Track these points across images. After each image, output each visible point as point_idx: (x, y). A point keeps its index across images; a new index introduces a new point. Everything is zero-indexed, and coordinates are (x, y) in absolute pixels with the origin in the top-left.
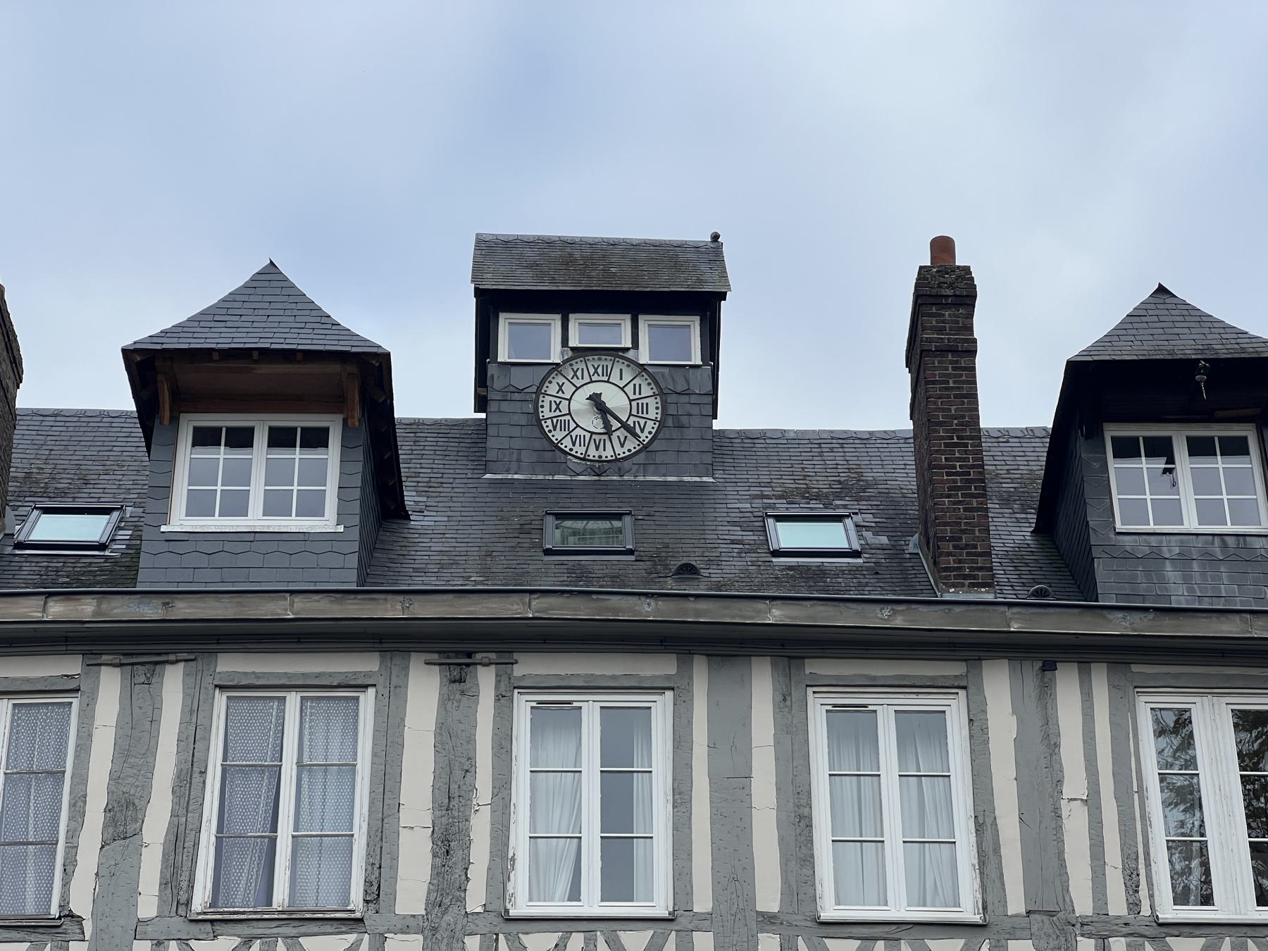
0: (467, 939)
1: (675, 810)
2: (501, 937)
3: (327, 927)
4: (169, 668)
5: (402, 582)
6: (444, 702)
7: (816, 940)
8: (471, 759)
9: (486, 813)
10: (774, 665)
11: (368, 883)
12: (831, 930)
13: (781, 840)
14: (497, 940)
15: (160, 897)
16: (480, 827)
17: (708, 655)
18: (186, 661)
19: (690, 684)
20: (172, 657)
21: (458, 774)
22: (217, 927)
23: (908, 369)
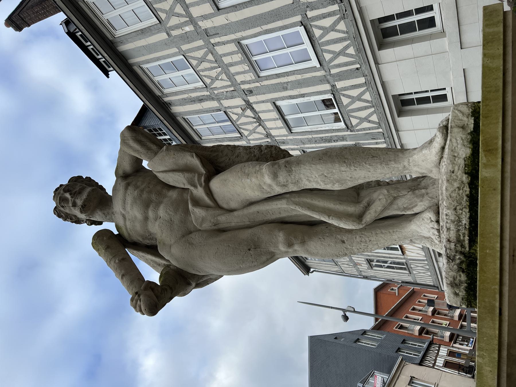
0: (216, 93)
1: (140, 32)
2: (211, 87)
3: (229, 117)
4: (165, 101)
5: (429, 356)
6: (176, 106)
7: (165, 23)
8: (182, 99)
9: (190, 95)
10: (118, 47)
11: (217, 111)
12: (160, 19)
13: (150, 36)
14: (212, 88)
15: (241, 141)
16: (194, 95)
17: (127, 60)
18: (161, 98)
19: (137, 63)
20: (162, 101)
21: (187, 101)
22: (241, 133)
23: (468, 366)
